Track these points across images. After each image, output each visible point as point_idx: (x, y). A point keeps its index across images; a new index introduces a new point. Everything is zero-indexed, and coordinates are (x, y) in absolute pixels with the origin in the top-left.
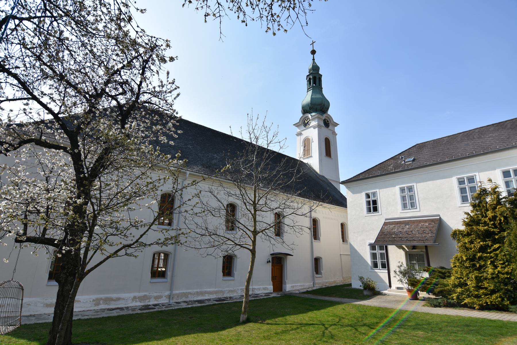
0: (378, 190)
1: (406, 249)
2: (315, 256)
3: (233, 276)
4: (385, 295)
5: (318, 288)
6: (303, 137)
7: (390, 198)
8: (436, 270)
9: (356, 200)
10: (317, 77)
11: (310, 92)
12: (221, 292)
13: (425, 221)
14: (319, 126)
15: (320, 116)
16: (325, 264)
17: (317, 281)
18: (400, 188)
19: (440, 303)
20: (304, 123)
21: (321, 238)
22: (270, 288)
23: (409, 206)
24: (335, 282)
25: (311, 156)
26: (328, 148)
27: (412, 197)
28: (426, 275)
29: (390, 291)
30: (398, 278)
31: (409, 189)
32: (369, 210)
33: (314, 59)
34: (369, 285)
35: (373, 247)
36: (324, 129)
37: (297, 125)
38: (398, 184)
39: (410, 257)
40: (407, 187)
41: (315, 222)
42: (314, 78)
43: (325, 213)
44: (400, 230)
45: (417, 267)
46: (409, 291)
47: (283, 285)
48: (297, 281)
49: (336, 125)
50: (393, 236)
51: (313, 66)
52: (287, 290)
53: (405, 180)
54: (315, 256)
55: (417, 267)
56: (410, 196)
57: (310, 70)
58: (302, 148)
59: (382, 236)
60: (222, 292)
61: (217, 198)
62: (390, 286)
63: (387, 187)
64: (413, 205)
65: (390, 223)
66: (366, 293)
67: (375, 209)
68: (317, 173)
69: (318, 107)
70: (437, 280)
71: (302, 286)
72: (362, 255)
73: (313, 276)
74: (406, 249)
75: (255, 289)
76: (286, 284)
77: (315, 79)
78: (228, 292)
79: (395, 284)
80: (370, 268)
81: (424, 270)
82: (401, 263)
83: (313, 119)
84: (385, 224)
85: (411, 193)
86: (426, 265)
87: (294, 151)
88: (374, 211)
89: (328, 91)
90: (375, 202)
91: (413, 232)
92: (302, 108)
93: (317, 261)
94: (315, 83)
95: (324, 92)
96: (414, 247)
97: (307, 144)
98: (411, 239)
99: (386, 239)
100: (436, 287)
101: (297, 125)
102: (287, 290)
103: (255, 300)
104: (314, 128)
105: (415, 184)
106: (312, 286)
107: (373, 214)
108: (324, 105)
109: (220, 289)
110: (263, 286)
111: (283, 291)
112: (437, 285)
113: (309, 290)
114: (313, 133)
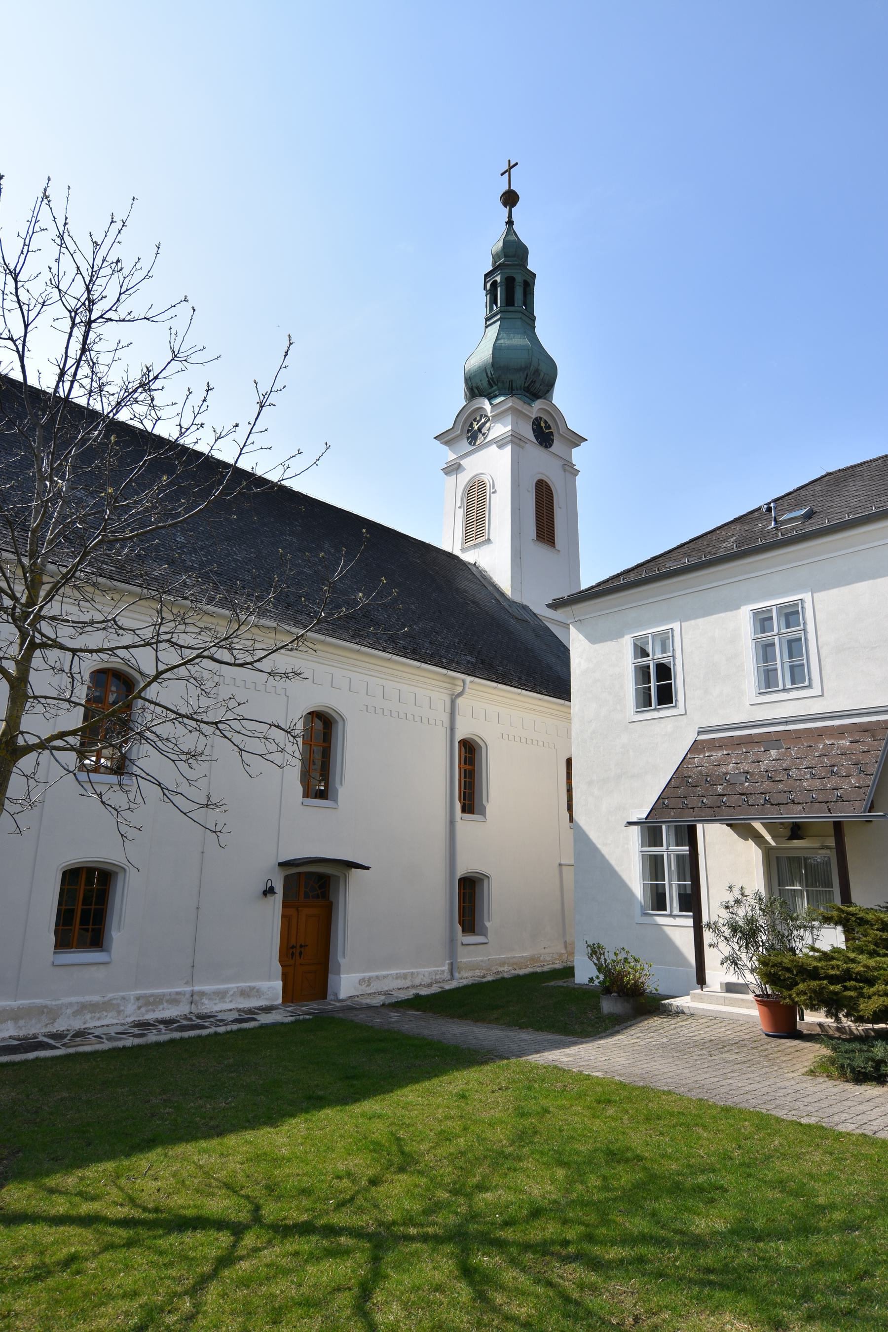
0: (676, 626)
1: (768, 838)
2: (465, 866)
3: (107, 950)
4: (679, 1013)
5: (465, 982)
6: (464, 478)
7: (716, 649)
8: (870, 917)
9: (599, 662)
10: (519, 279)
11: (494, 329)
12: (42, 1011)
13: (840, 732)
14: (516, 439)
15: (525, 408)
16: (498, 902)
17: (465, 957)
18: (756, 613)
19: (879, 1063)
20: (469, 430)
21: (490, 808)
22: (272, 988)
23: (783, 677)
24: (533, 959)
25: (488, 541)
26: (545, 515)
27: (794, 646)
28: (832, 938)
29: (700, 999)
30: (726, 949)
31: (788, 616)
32: (644, 700)
33: (510, 223)
34: (621, 975)
35: (651, 832)
36: (535, 451)
37: (446, 438)
38: (748, 600)
39: (778, 867)
40: (780, 608)
41: (469, 754)
42: (509, 283)
43: (495, 711)
44: (746, 766)
45: (803, 905)
46: (763, 1000)
47: (331, 977)
48: (383, 957)
49: (577, 440)
50: (719, 789)
51: (506, 243)
52: (343, 995)
53: (770, 583)
54: (460, 872)
55: (803, 905)
56: (790, 643)
57: (496, 257)
58: (460, 513)
59: (681, 792)
60: (53, 1013)
61: (91, 651)
62: (701, 980)
63: (707, 612)
64: (798, 675)
65: (713, 745)
66: (608, 1006)
67: (666, 696)
68: (502, 594)
69: (518, 378)
70: (871, 963)
71: (405, 976)
72: (613, 862)
73: (452, 940)
74: (768, 838)
75: (202, 994)
76: (339, 973)
77: (511, 286)
78: (75, 1014)
79: (718, 974)
80: (638, 911)
81: (827, 920)
82: (736, 894)
83: (498, 417)
84: (697, 747)
85: (793, 632)
86: (838, 901)
87: (438, 528)
88: (661, 702)
89: (554, 325)
90: (664, 671)
91: (794, 773)
92: (466, 380)
93: (469, 892)
94: (509, 300)
95: (542, 330)
96: (796, 831)
97: (476, 497)
98: (783, 798)
99: (693, 801)
100: (867, 990)
101: (446, 438)
102: (343, 995)
103: (239, 1030)
104: (500, 443)
105: (807, 597)
106: (447, 975)
107: (655, 714)
108: (537, 372)
109: (38, 1001)
110: (248, 982)
111: (330, 997)
112: (871, 982)
113: (424, 992)
114: (494, 463)
